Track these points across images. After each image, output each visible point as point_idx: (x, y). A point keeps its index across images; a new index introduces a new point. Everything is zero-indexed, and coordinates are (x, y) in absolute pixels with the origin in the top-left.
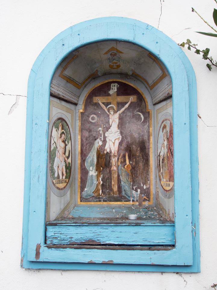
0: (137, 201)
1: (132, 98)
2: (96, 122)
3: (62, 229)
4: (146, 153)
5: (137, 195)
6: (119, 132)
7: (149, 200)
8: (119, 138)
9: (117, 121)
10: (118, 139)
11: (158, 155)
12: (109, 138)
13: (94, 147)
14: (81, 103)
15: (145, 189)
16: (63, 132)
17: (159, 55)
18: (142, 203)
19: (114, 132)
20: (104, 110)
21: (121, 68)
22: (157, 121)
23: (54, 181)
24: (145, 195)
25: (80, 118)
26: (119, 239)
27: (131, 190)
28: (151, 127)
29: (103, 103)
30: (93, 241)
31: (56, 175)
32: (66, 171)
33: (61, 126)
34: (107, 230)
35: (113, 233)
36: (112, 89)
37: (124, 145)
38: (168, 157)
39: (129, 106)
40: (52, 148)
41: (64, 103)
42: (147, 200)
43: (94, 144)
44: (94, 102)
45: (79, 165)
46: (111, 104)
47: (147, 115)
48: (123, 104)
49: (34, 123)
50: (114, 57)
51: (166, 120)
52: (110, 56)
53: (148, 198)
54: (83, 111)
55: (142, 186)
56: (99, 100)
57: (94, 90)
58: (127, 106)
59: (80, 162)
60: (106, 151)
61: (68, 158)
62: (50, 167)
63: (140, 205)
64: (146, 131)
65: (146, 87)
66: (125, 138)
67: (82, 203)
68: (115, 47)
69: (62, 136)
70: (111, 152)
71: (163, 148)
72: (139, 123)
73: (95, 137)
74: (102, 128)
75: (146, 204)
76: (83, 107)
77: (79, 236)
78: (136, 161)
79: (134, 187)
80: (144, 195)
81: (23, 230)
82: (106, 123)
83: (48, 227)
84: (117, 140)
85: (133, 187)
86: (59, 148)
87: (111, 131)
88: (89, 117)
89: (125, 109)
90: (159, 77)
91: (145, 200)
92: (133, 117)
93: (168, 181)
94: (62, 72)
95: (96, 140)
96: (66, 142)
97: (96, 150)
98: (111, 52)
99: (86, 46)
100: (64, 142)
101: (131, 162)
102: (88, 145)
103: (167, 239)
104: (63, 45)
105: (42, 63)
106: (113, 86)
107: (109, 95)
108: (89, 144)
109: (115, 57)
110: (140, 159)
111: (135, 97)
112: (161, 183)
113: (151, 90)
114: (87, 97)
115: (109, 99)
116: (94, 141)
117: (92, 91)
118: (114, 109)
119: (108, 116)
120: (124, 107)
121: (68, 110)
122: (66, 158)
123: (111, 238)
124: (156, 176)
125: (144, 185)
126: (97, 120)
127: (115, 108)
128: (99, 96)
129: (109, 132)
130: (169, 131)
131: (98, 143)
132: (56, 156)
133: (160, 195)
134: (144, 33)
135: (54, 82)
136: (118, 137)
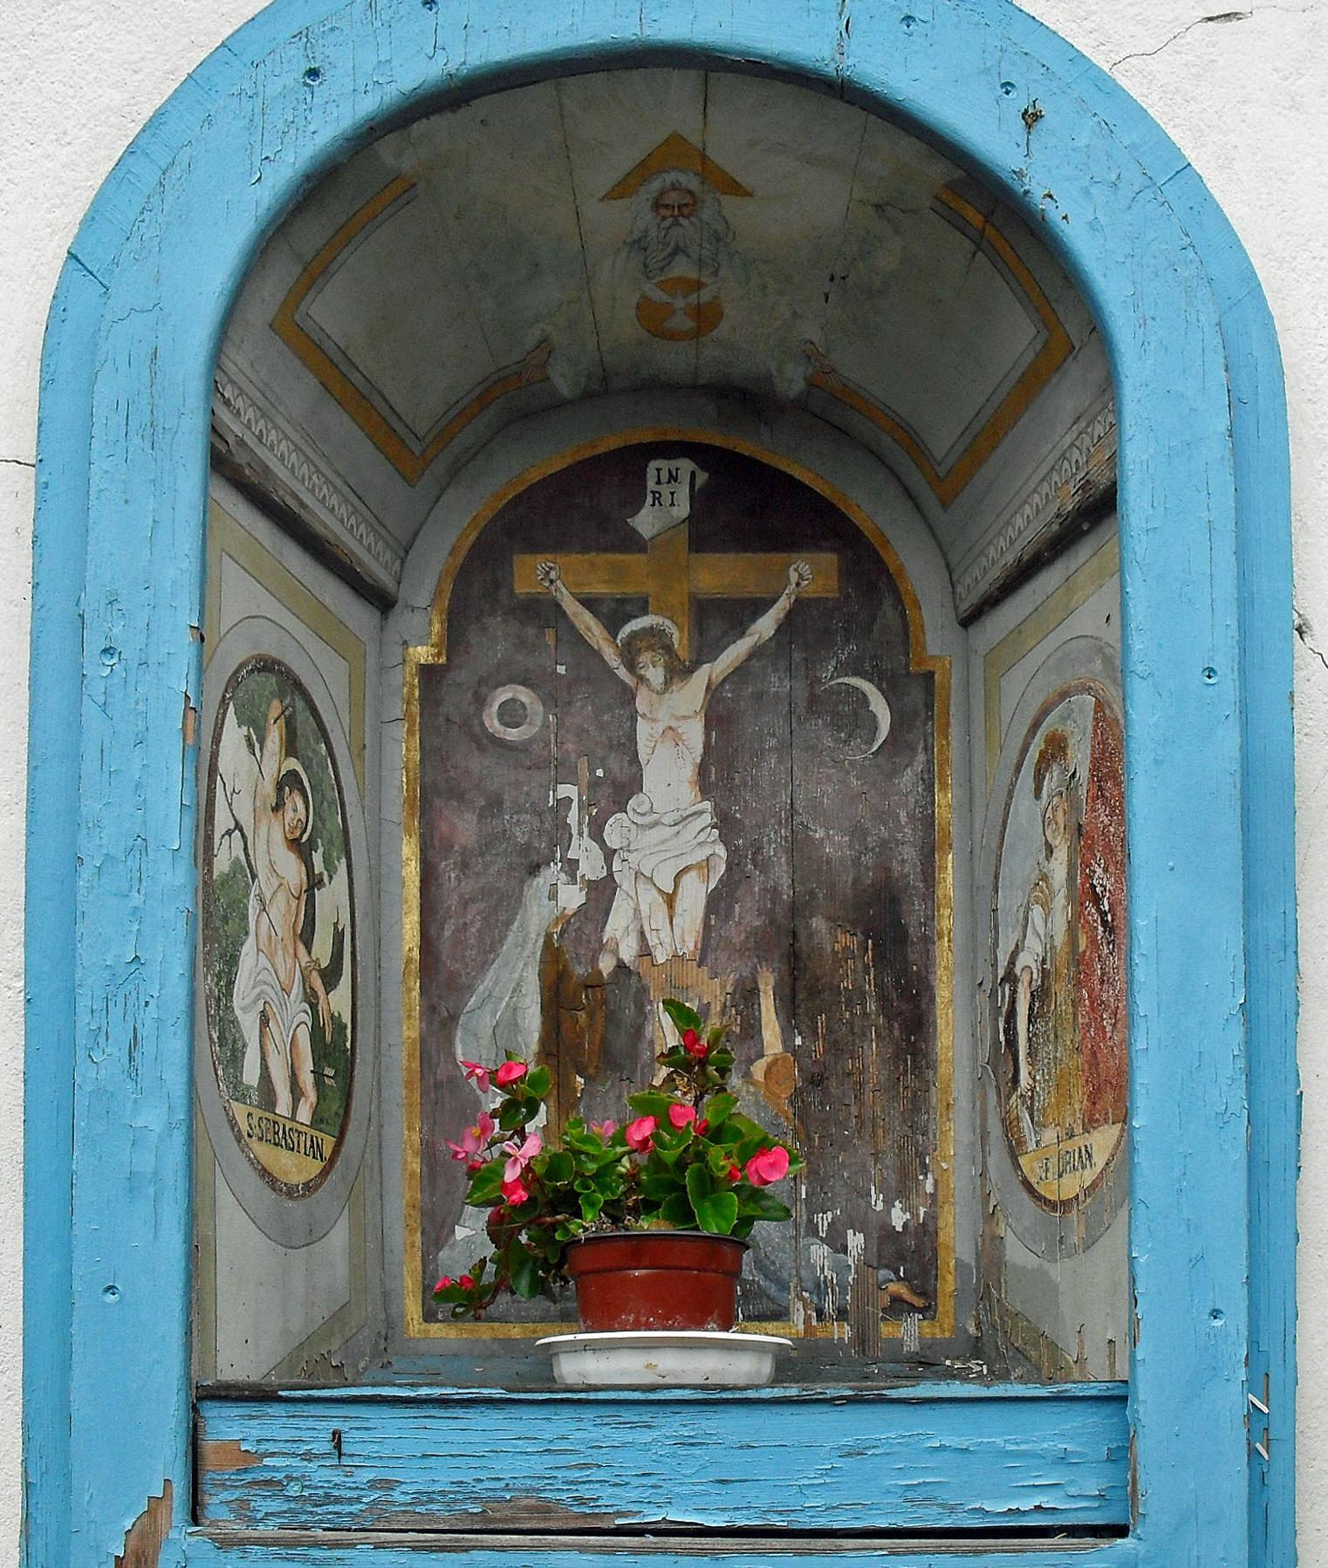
0: (842, 1314)
1: (805, 569)
2: (531, 741)
3: (310, 1423)
4: (905, 971)
5: (842, 1269)
6: (707, 819)
7: (928, 1311)
8: (706, 865)
9: (694, 733)
10: (698, 866)
11: (1001, 973)
12: (632, 857)
13: (524, 928)
14: (423, 599)
15: (899, 1229)
16: (293, 774)
17: (1019, 174)
18: (877, 1330)
19: (667, 820)
20: (597, 654)
21: (723, 330)
22: (987, 735)
23: (239, 1111)
24: (897, 1272)
25: (416, 709)
26: (732, 1496)
27: (796, 1238)
28: (944, 787)
29: (589, 603)
30: (545, 1509)
31: (251, 1075)
32: (318, 1074)
33: (282, 721)
34: (646, 1436)
35: (696, 1451)
36: (657, 497)
37: (747, 915)
38: (1077, 960)
39: (778, 631)
40: (222, 865)
41: (295, 559)
42: (914, 1309)
43: (519, 901)
44: (521, 589)
45: (410, 1056)
46: (644, 611)
47: (916, 696)
48: (742, 612)
49: (94, 644)
50: (676, 224)
51: (1064, 695)
52: (648, 218)
53: (923, 1294)
54: (439, 655)
55: (880, 1206)
56: (553, 575)
57: (518, 498)
58: (765, 626)
59: (414, 1034)
60: (615, 952)
61: (331, 977)
62: (208, 997)
63: (862, 1340)
64: (911, 817)
65: (910, 495)
66: (754, 861)
67: (436, 1329)
68: (694, 139)
69: (289, 805)
70: (645, 952)
71: (1037, 913)
72: (858, 753)
73: (526, 849)
74: (585, 787)
75: (909, 1332)
76: (436, 627)
77: (442, 1477)
78: (830, 1030)
79: (823, 1221)
80: (892, 1276)
81: (26, 1427)
82: (611, 747)
83: (210, 1411)
84: (693, 874)
85: (810, 1221)
86: (265, 883)
87: (645, 808)
88: (481, 702)
89: (756, 653)
90: (1015, 376)
91: (898, 1308)
92: (813, 713)
93: (1078, 1130)
94: (295, 297)
95: (534, 870)
96: (317, 858)
97: (536, 946)
98: (656, 185)
99: (481, 106)
100: (301, 848)
101: (798, 1041)
102: (473, 909)
103: (1073, 1491)
104: (313, 73)
105: (155, 200)
106: (665, 476)
107: (632, 542)
108: (482, 905)
109: (687, 230)
110: (865, 1014)
111: (829, 560)
112: (1017, 1166)
113: (945, 505)
114: (463, 552)
115: (637, 573)
116: (522, 882)
117: (503, 511)
118: (668, 649)
119: (628, 696)
120: (742, 634)
121: (326, 627)
122: (315, 974)
123: (677, 1490)
124: (984, 1136)
125: (889, 1204)
126: (545, 725)
127: (677, 638)
128: (559, 544)
129: (639, 820)
130: (1084, 773)
131: (553, 896)
132: (247, 934)
133: (1016, 1253)
134: (916, 15)
135: (238, 360)
136: (700, 855)
